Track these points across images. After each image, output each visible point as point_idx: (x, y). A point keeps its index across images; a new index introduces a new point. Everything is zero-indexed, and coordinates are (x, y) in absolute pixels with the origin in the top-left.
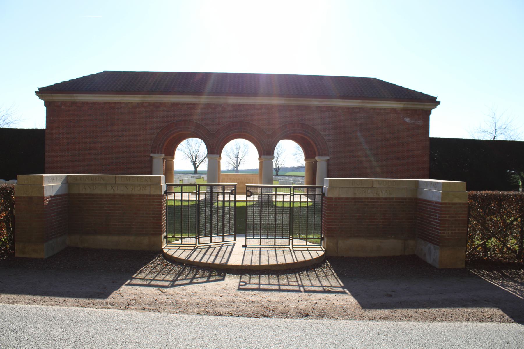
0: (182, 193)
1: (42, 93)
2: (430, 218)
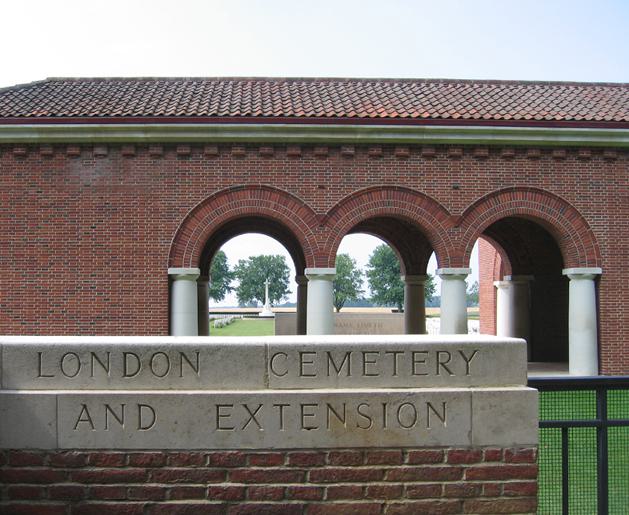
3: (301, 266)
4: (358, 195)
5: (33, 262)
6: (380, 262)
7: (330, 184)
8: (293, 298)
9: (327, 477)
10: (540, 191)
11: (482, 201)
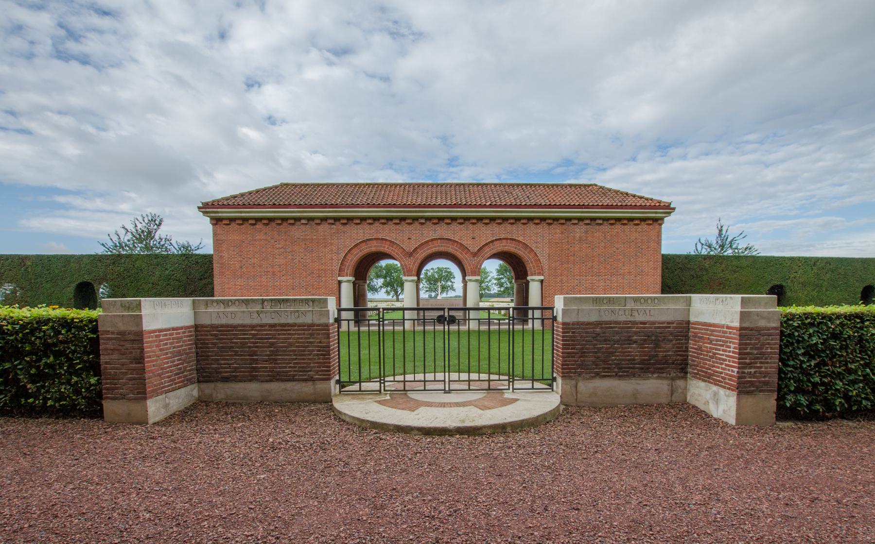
0: (469, 373)
1: (206, 208)
2: (716, 349)
3: (464, 274)
4: (427, 242)
5: (274, 274)
6: (500, 271)
7: (413, 237)
8: (459, 292)
9: (277, 330)
10: (514, 240)
11: (486, 244)
